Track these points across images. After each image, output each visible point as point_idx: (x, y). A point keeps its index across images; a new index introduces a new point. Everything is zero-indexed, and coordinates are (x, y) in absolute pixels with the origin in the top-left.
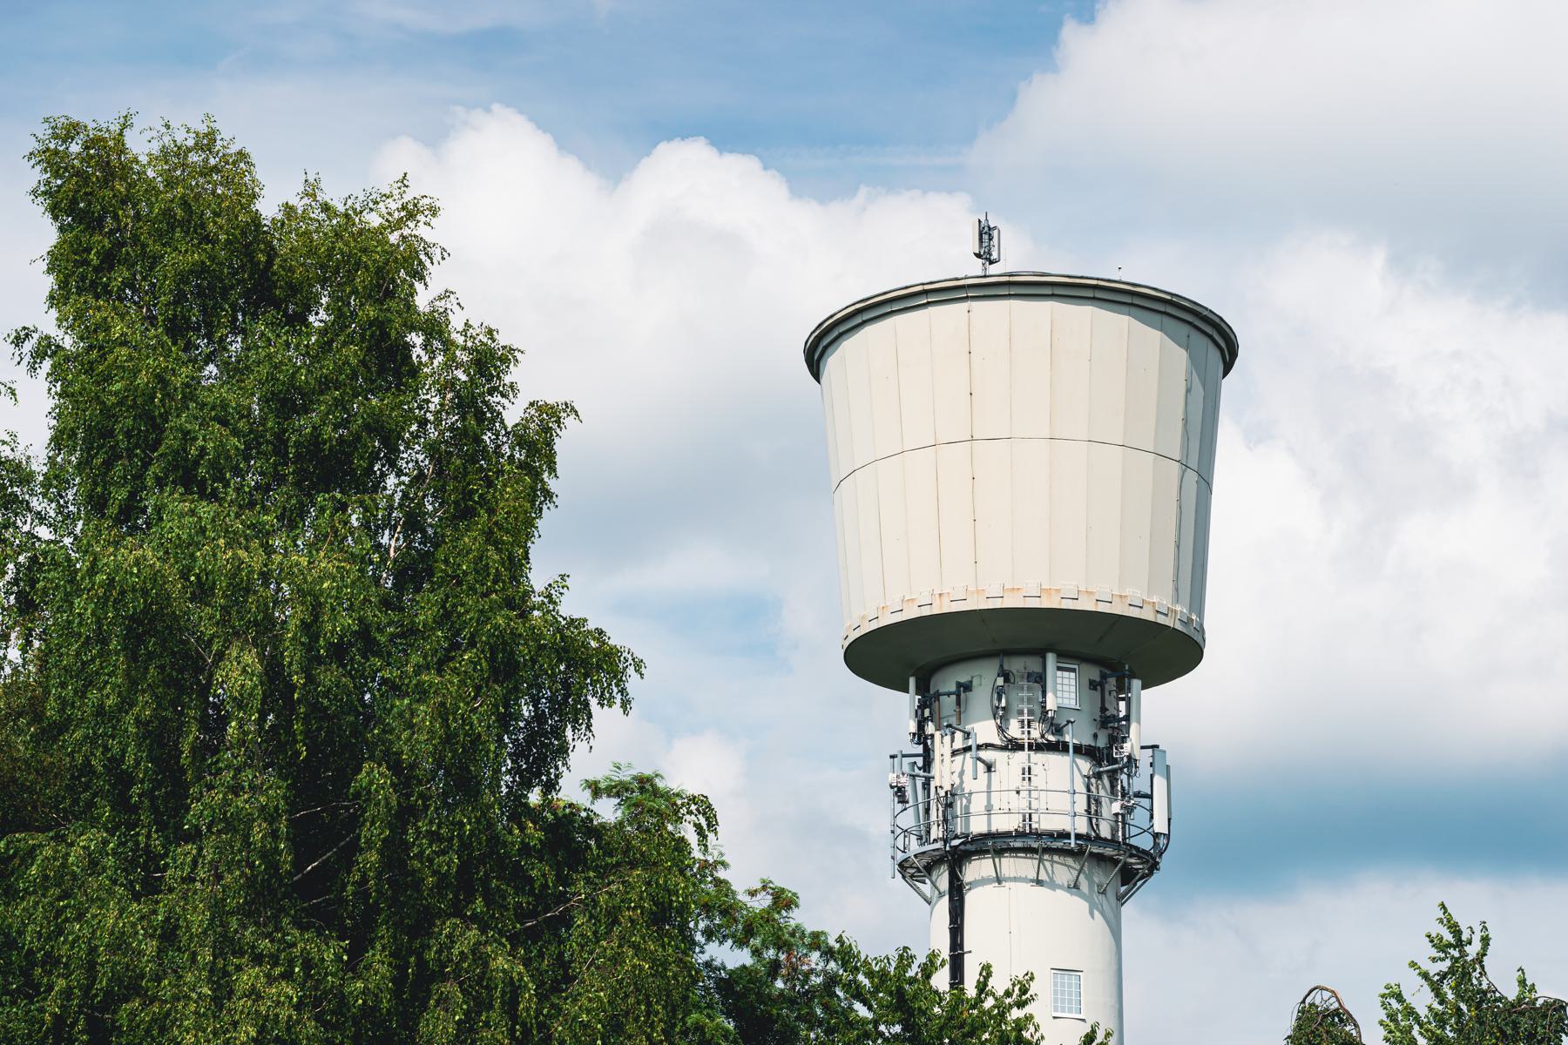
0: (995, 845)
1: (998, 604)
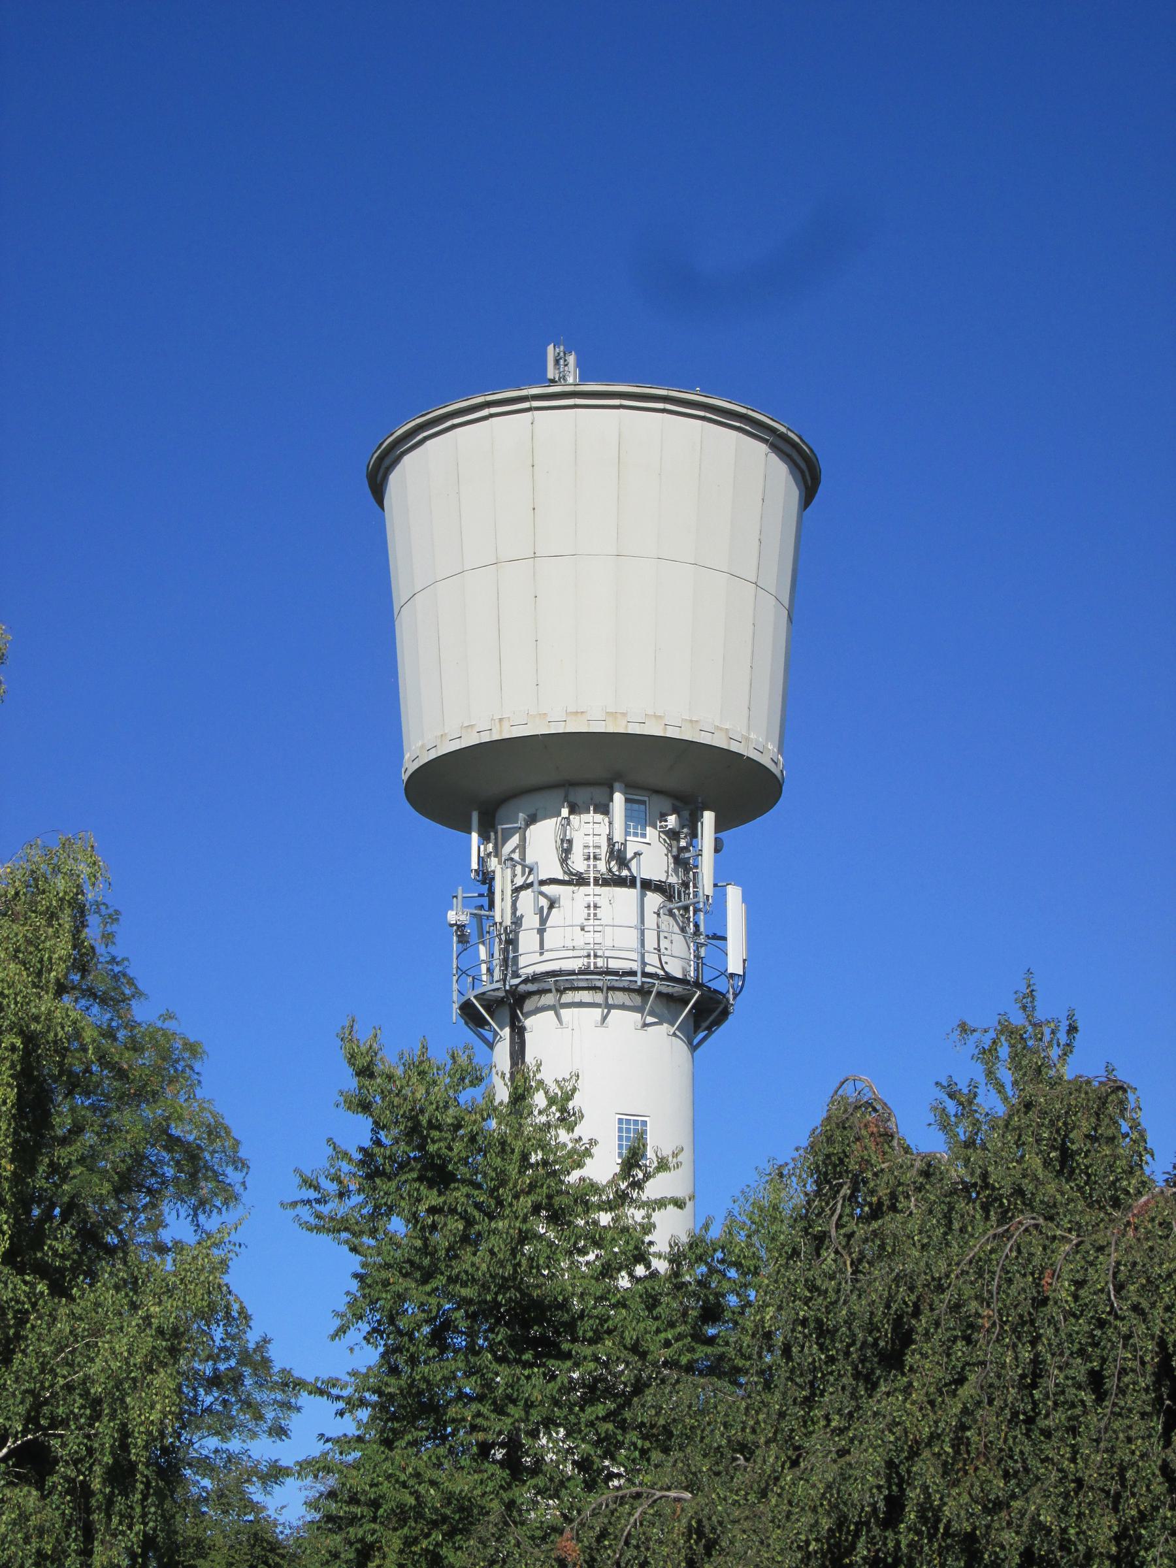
0: (556, 984)
1: (561, 729)
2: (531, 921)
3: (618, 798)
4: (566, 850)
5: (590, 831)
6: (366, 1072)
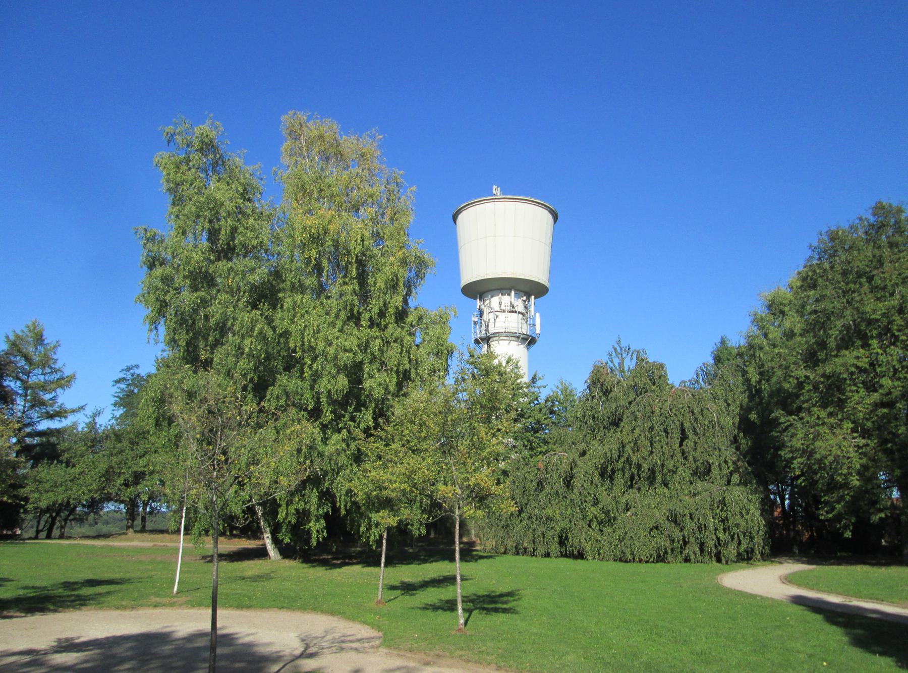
3: (513, 292)
4: (500, 304)
5: (506, 300)
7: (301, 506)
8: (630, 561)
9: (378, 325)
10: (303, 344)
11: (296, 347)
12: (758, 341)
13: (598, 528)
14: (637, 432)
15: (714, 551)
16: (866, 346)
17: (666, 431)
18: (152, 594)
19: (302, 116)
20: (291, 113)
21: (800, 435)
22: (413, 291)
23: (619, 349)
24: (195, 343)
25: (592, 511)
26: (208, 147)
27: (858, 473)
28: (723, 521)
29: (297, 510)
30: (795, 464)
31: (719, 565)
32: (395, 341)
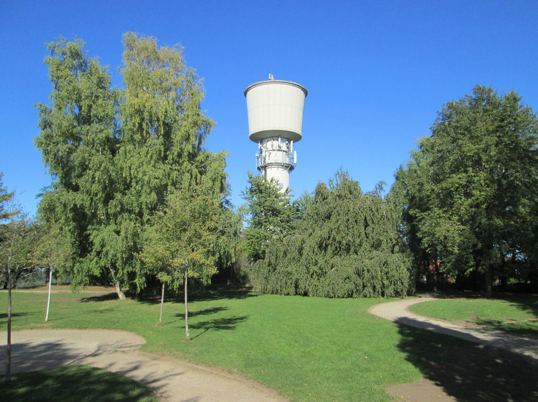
2: (267, 156)
3: (280, 139)
4: (272, 146)
5: (276, 143)
6: (251, 178)
7: (130, 269)
8: (332, 297)
9: (178, 162)
10: (130, 174)
11: (126, 176)
12: (413, 168)
13: (317, 278)
14: (339, 222)
15: (380, 291)
16: (466, 172)
17: (356, 221)
18: (33, 321)
19: (134, 35)
20: (128, 33)
21: (427, 224)
22: (203, 141)
23: (340, 173)
24: (68, 173)
25: (313, 268)
26: (76, 55)
27: (458, 246)
28: (386, 274)
29: (128, 272)
30: (425, 240)
31: (382, 298)
32: (188, 172)
